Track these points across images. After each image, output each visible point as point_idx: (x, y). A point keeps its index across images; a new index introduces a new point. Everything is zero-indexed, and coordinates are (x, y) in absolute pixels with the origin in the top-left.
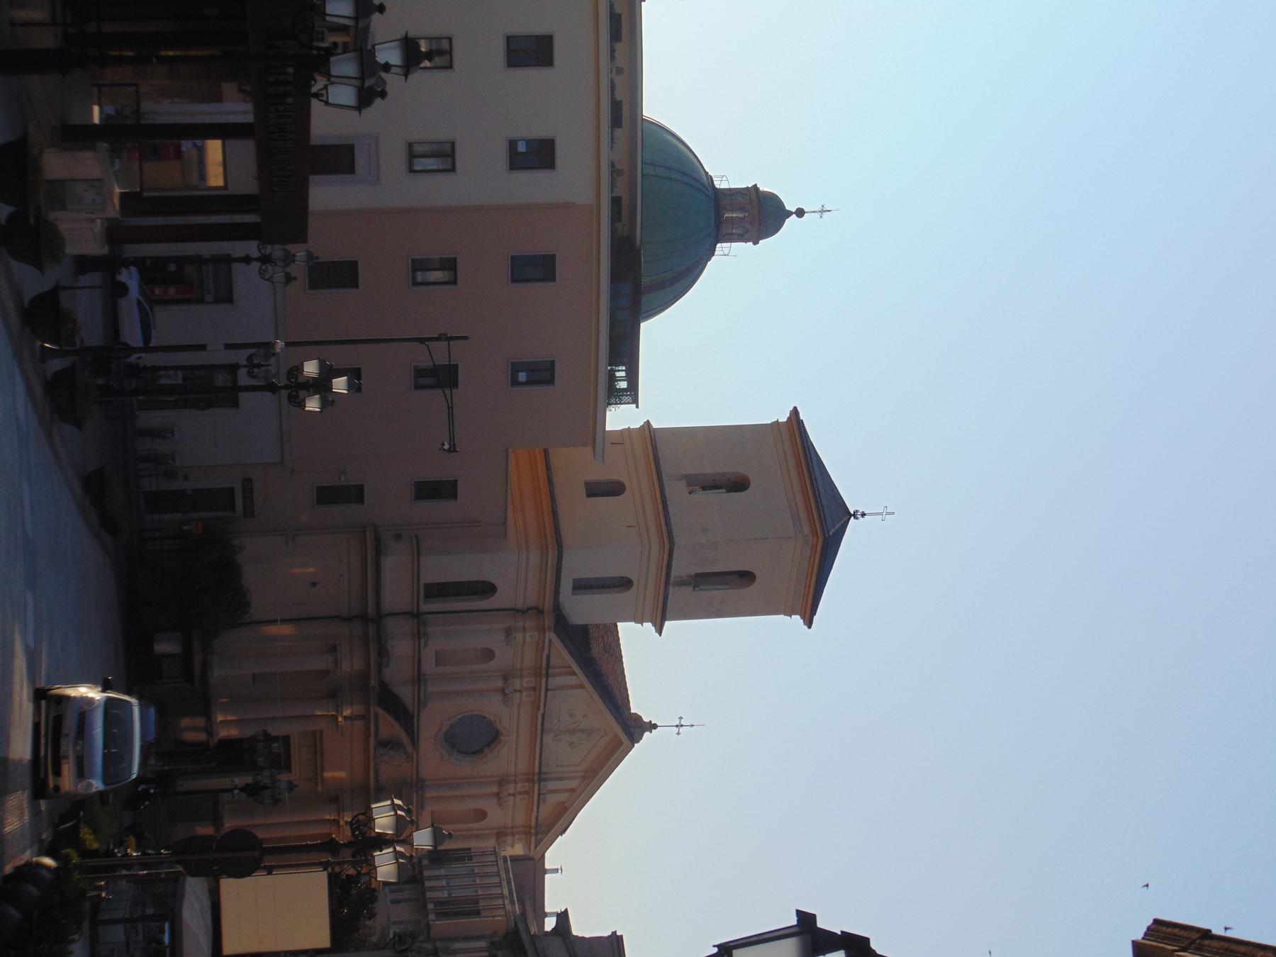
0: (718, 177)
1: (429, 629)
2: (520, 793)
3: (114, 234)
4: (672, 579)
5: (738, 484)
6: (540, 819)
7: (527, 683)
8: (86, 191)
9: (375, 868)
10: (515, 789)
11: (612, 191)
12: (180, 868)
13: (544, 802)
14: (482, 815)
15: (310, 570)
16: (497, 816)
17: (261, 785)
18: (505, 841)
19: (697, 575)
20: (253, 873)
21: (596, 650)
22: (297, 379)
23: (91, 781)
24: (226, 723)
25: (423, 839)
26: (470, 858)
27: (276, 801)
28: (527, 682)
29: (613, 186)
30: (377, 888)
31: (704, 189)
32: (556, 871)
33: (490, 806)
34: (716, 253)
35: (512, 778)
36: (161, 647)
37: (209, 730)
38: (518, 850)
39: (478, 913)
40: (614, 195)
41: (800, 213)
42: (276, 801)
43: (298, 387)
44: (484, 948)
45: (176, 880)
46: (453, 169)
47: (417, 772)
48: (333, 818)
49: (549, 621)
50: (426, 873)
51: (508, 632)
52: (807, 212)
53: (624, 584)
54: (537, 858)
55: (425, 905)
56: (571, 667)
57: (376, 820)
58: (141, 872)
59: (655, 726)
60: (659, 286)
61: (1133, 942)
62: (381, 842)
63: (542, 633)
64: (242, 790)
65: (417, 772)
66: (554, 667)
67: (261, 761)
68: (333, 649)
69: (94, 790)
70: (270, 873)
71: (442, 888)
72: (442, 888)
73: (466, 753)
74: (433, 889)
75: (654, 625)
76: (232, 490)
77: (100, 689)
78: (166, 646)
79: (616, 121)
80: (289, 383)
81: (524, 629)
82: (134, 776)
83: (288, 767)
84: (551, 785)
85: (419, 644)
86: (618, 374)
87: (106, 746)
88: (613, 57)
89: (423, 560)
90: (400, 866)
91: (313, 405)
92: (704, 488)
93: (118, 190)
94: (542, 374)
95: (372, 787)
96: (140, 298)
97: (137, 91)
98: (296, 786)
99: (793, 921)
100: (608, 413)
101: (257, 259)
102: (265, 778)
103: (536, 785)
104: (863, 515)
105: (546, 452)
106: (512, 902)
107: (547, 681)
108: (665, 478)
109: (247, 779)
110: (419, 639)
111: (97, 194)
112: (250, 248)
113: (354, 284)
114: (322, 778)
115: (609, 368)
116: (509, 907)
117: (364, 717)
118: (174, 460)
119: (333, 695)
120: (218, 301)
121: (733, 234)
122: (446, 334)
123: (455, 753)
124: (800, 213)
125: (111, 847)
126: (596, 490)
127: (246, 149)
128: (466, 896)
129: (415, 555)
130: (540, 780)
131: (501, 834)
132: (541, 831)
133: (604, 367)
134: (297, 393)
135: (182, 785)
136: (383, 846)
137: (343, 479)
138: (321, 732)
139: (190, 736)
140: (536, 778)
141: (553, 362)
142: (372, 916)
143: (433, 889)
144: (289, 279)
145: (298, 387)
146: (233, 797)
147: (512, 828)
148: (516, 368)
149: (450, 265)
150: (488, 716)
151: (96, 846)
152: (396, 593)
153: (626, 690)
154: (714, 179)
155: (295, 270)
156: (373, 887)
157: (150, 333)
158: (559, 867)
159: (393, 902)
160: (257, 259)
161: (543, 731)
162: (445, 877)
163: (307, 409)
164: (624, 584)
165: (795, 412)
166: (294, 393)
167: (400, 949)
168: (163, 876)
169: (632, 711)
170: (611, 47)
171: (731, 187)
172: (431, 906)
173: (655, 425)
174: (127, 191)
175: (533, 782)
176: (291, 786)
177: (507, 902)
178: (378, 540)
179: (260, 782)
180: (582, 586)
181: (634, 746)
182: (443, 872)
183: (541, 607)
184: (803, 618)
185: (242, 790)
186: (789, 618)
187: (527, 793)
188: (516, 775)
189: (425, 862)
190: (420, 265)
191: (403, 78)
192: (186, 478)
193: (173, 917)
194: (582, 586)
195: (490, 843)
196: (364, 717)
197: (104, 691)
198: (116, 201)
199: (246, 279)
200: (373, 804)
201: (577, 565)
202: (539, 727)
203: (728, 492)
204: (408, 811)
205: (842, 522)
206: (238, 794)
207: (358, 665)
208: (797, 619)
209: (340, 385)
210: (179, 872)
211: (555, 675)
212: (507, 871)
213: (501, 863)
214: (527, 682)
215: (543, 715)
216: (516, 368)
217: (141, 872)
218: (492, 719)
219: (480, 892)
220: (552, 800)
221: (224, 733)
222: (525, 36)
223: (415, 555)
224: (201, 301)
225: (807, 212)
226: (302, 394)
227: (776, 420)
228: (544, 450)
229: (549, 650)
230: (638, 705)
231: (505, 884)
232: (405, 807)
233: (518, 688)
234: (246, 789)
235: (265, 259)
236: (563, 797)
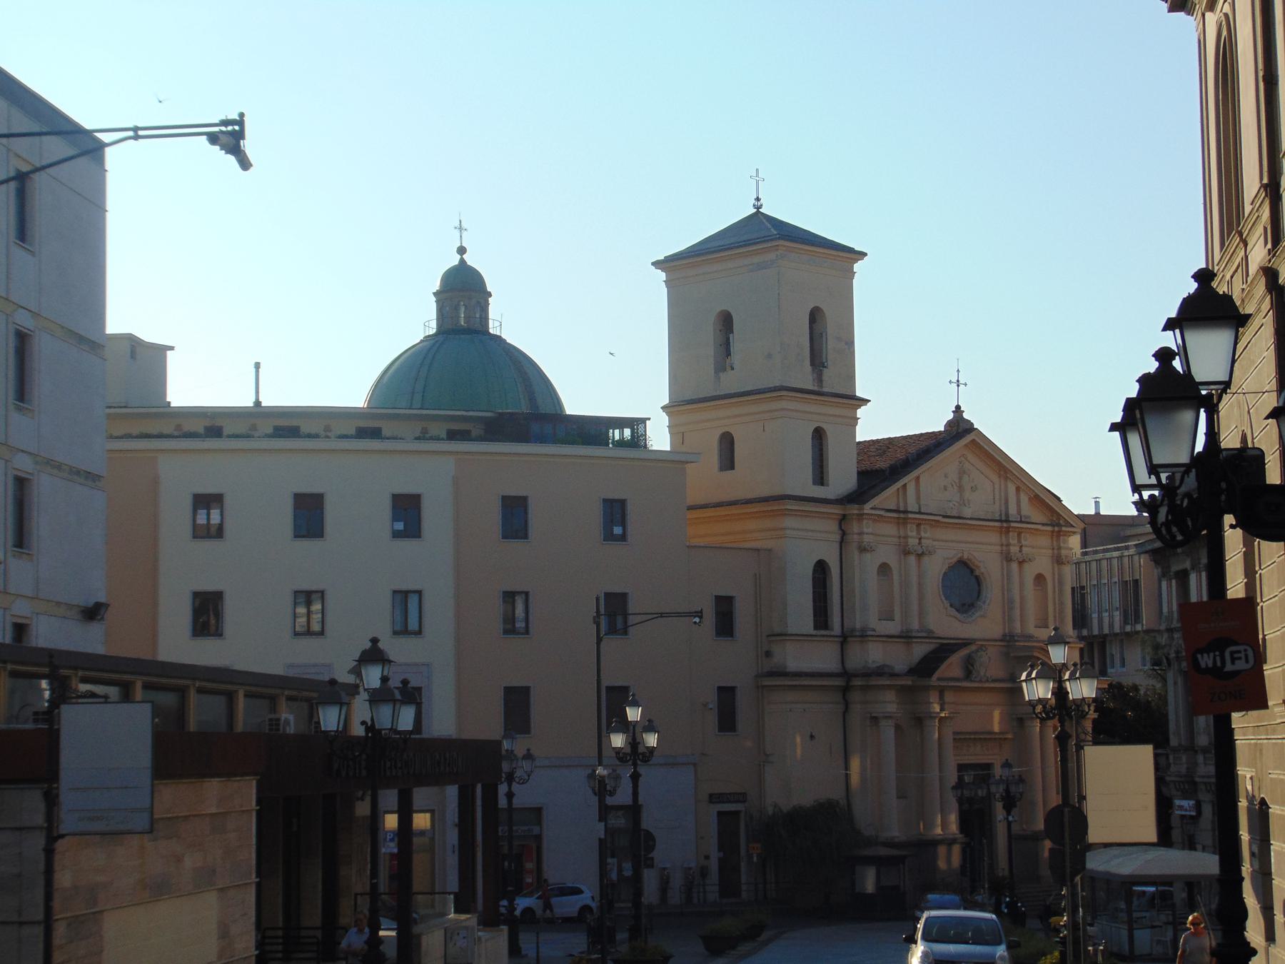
0: (425, 332)
1: (858, 626)
2: (1019, 541)
3: (490, 920)
4: (816, 388)
5: (726, 322)
6: (1045, 520)
8: (455, 944)
9: (1084, 699)
10: (1014, 545)
11: (443, 439)
12: (1078, 878)
13: (1029, 517)
14: (1040, 579)
15: (798, 740)
16: (1042, 564)
17: (1004, 794)
18: (1066, 557)
19: (813, 363)
20: (1083, 813)
21: (882, 464)
22: (628, 754)
23: (998, 955)
24: (944, 825)
25: (1058, 655)
26: (1083, 588)
27: (1021, 780)
28: (912, 531)
29: (438, 439)
30: (1109, 682)
31: (437, 345)
32: (1097, 503)
33: (1030, 571)
34: (499, 334)
35: (1004, 548)
36: (870, 886)
37: (950, 842)
38: (1074, 542)
39: (1136, 582)
40: (445, 437)
41: (462, 250)
42: (1021, 780)
43: (636, 753)
44: (1167, 584)
45: (1094, 880)
46: (419, 593)
47: (996, 640)
48: (1039, 725)
49: (853, 509)
50: (1096, 632)
51: (863, 550)
52: (461, 243)
53: (819, 435)
54: (1082, 525)
55: (1127, 634)
56: (898, 489)
57: (1040, 697)
58: (1081, 914)
59: (958, 407)
60: (532, 399)
61: (1169, 11)
62: (1060, 693)
63: (864, 517)
64: (1009, 813)
65: (996, 640)
66: (898, 504)
67: (981, 793)
68: (875, 720)
69: (1006, 954)
70: (1084, 798)
71: (1111, 617)
72: (1111, 617)
73: (979, 592)
74: (1111, 626)
75: (859, 406)
76: (720, 814)
77: (914, 946)
78: (869, 881)
79: (375, 433)
80: (631, 761)
81: (861, 534)
82: (994, 916)
83: (988, 766)
84: (1013, 511)
85: (872, 636)
86: (617, 437)
87: (967, 943)
88: (316, 436)
89: (790, 631)
90: (1082, 676)
91: (652, 740)
92: (728, 354)
93: (452, 916)
94: (615, 511)
95: (1009, 685)
96: (536, 896)
97: (361, 894)
98: (1007, 760)
99: (1117, 434)
100: (655, 448)
101: (510, 786)
102: (998, 790)
103: (1013, 525)
104: (758, 199)
105: (691, 508)
106: (1127, 548)
107: (911, 512)
108: (718, 393)
109: (999, 808)
110: (867, 636)
111: (458, 934)
112: (503, 789)
113: (525, 691)
114: (1000, 733)
115: (611, 446)
116: (1132, 551)
117: (942, 691)
118: (690, 869)
119: (920, 721)
120: (539, 822)
121: (481, 318)
122: (594, 617)
123: (979, 603)
124: (462, 250)
125: (1058, 939)
126: (728, 462)
127: (421, 795)
128: (1119, 594)
129: (787, 638)
130: (1007, 521)
131: (1059, 560)
132: (1057, 522)
133: (610, 451)
134: (641, 754)
135: (1003, 869)
136: (1064, 691)
137: (711, 706)
139: (956, 860)
140: (1005, 525)
141: (605, 500)
142: (1135, 688)
143: (1111, 626)
144: (528, 756)
145: (636, 753)
146: (1015, 821)
147: (1053, 549)
148: (609, 537)
149: (509, 597)
150: (944, 571)
151: (1057, 954)
152: (822, 657)
153: (922, 434)
154: (427, 334)
155: (520, 750)
156: (1106, 686)
157: (569, 887)
158: (1094, 500)
159: (1123, 665)
160: (510, 786)
161: (959, 518)
162: (1100, 613)
163: (655, 746)
164: (819, 435)
165: (657, 264)
166: (641, 757)
167: (1166, 664)
168: (1084, 894)
169: (943, 429)
170: (305, 437)
171: (435, 317)
172: (1128, 628)
173: (666, 401)
174: (453, 905)
175: (1008, 528)
176: (1007, 765)
177: (1126, 553)
178: (772, 674)
179: (1002, 796)
180: (820, 477)
181: (977, 429)
182: (1095, 616)
183: (840, 517)
184: (856, 261)
185: (1009, 813)
186: (856, 274)
187: (1019, 534)
188: (1002, 545)
189: (1085, 632)
190: (510, 628)
191: (392, 663)
192: (707, 857)
193: (1128, 883)
194: (820, 477)
195: (1068, 571)
196: (942, 691)
197: (916, 943)
198: (463, 917)
199: (525, 796)
200: (1025, 699)
201: (801, 482)
202: (954, 520)
204: (1033, 667)
205: (764, 221)
206: (1013, 817)
207: (890, 696)
208: (857, 267)
209: (633, 714)
210: (1081, 879)
212: (1096, 552)
213: (1087, 558)
214: (912, 531)
215: (944, 517)
216: (609, 537)
217: (1081, 914)
218: (947, 566)
220: (1027, 509)
221: (954, 827)
222: (295, 521)
223: (787, 638)
224: (538, 838)
225: (461, 243)
226: (641, 749)
227: (664, 283)
228: (688, 510)
229: (883, 509)
230: (936, 423)
231: (1108, 555)
232: (1029, 670)
233: (917, 541)
234: (1009, 807)
235: (510, 778)
236: (1024, 499)
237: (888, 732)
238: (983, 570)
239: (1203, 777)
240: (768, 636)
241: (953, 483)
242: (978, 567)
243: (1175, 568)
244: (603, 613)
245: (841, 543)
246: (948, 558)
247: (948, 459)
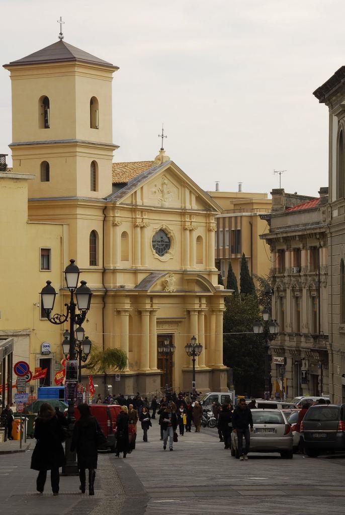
5: (45, 102)
7: (139, 215)
53: (94, 165)
56: (132, 194)
66: (132, 201)
68: (119, 312)
104: (61, 34)
137: (39, 305)
138: (157, 319)
172: (233, 256)
203: (49, 108)
207: (128, 301)
211: (136, 202)
219: (227, 229)
237: (126, 319)
238: (172, 234)
239: (288, 347)
242: (170, 233)
243: (278, 248)
245: (104, 221)
247: (157, 178)
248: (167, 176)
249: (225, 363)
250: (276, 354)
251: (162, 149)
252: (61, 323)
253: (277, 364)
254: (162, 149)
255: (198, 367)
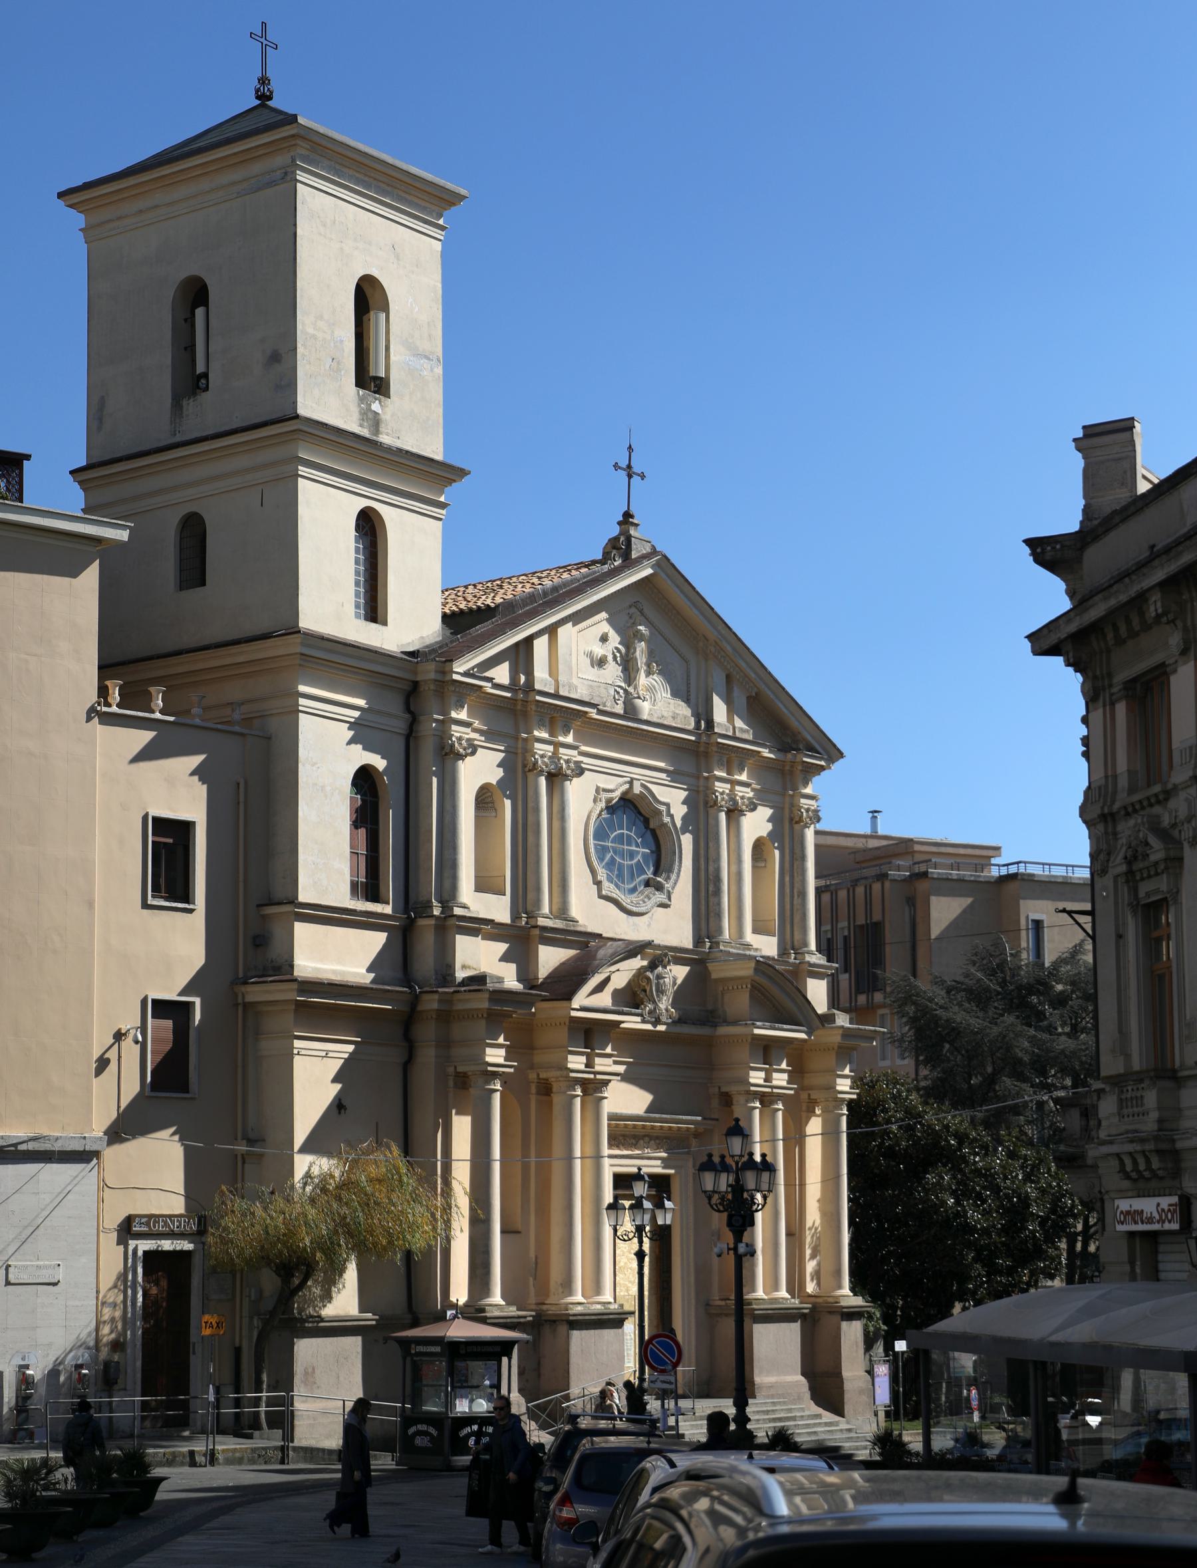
104: (264, 80)
240: (258, 906)
241: (618, 689)
244: (468, 1351)
246: (605, 790)
248: (646, 611)
249: (857, 1287)
250: (1126, 1184)
251: (627, 515)
252: (630, 1240)
253: (1131, 1234)
254: (627, 515)
255: (518, 698)
